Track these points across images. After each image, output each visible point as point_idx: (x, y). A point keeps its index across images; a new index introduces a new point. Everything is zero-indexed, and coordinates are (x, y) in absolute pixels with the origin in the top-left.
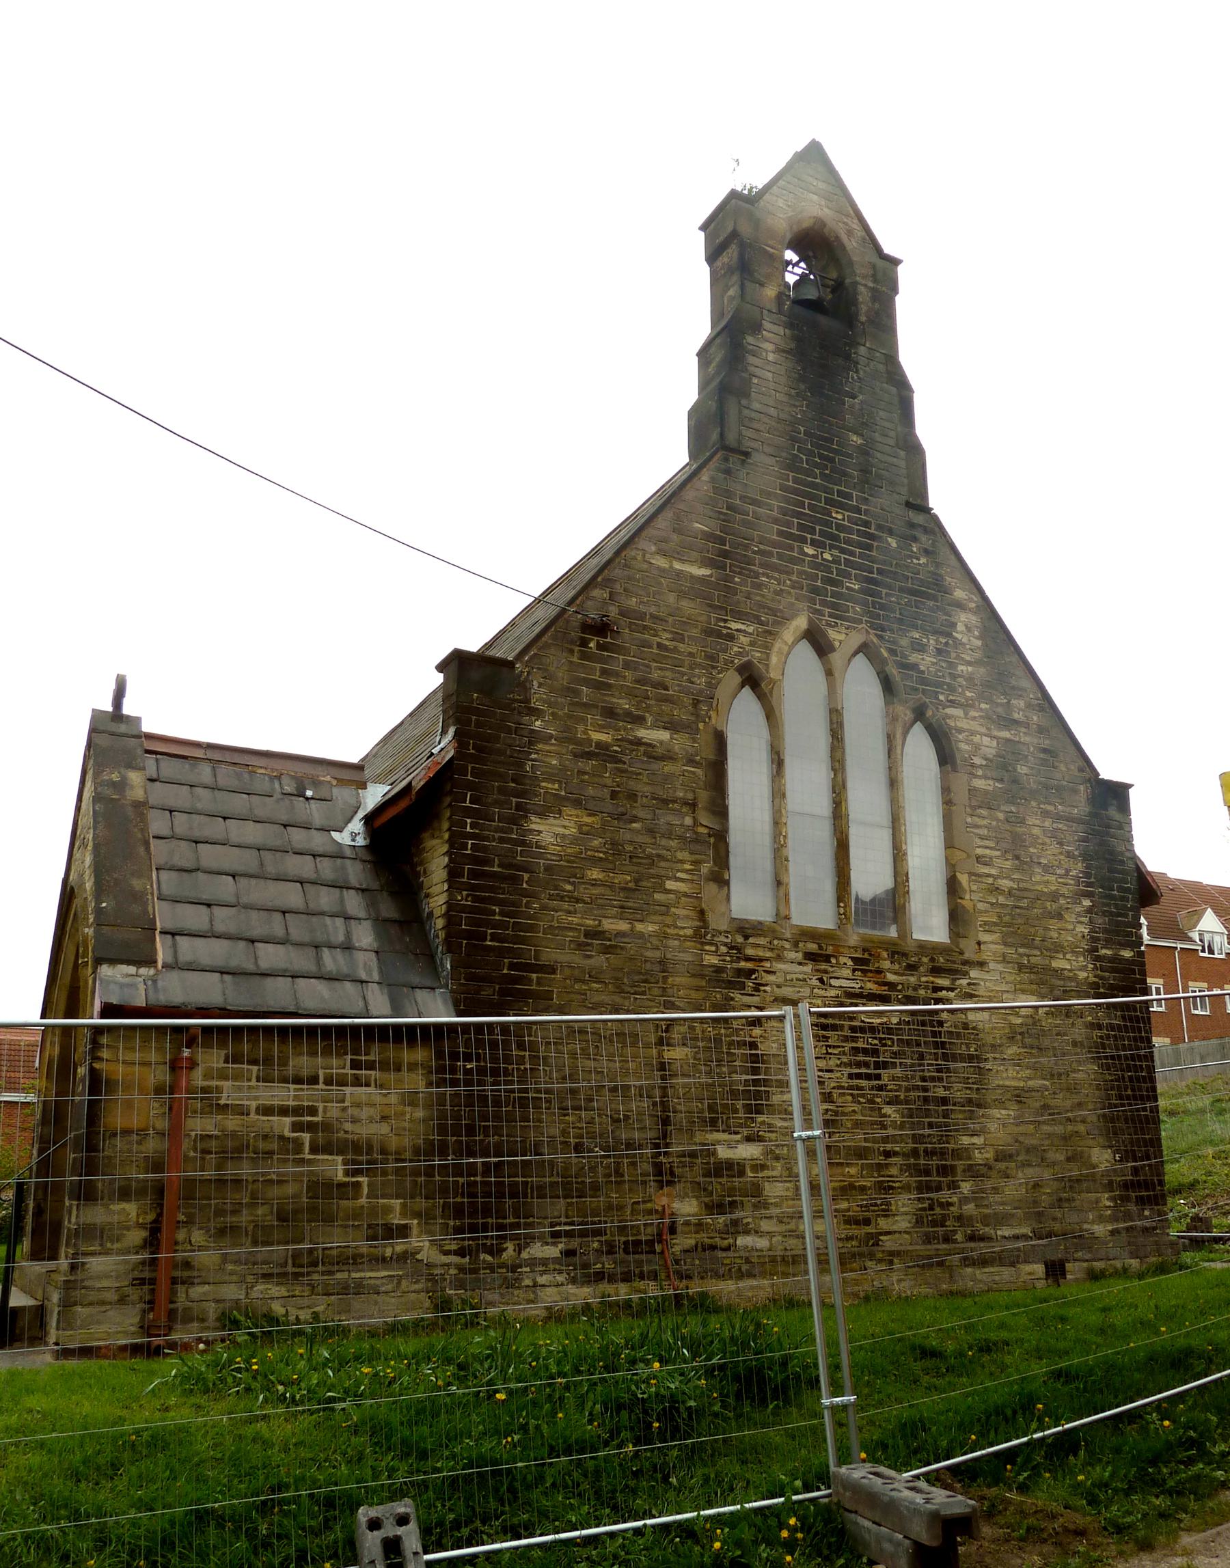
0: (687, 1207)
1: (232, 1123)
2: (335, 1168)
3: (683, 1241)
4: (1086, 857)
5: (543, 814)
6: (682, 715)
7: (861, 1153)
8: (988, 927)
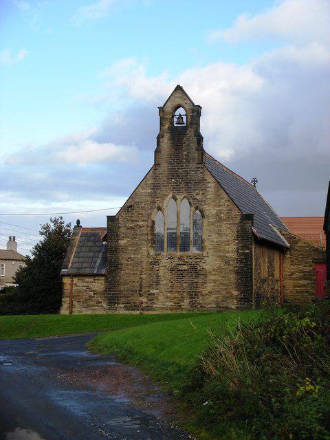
0: (144, 300)
1: (79, 288)
2: (92, 294)
3: (144, 305)
4: (238, 231)
5: (121, 240)
6: (145, 219)
7: (178, 292)
8: (210, 249)
